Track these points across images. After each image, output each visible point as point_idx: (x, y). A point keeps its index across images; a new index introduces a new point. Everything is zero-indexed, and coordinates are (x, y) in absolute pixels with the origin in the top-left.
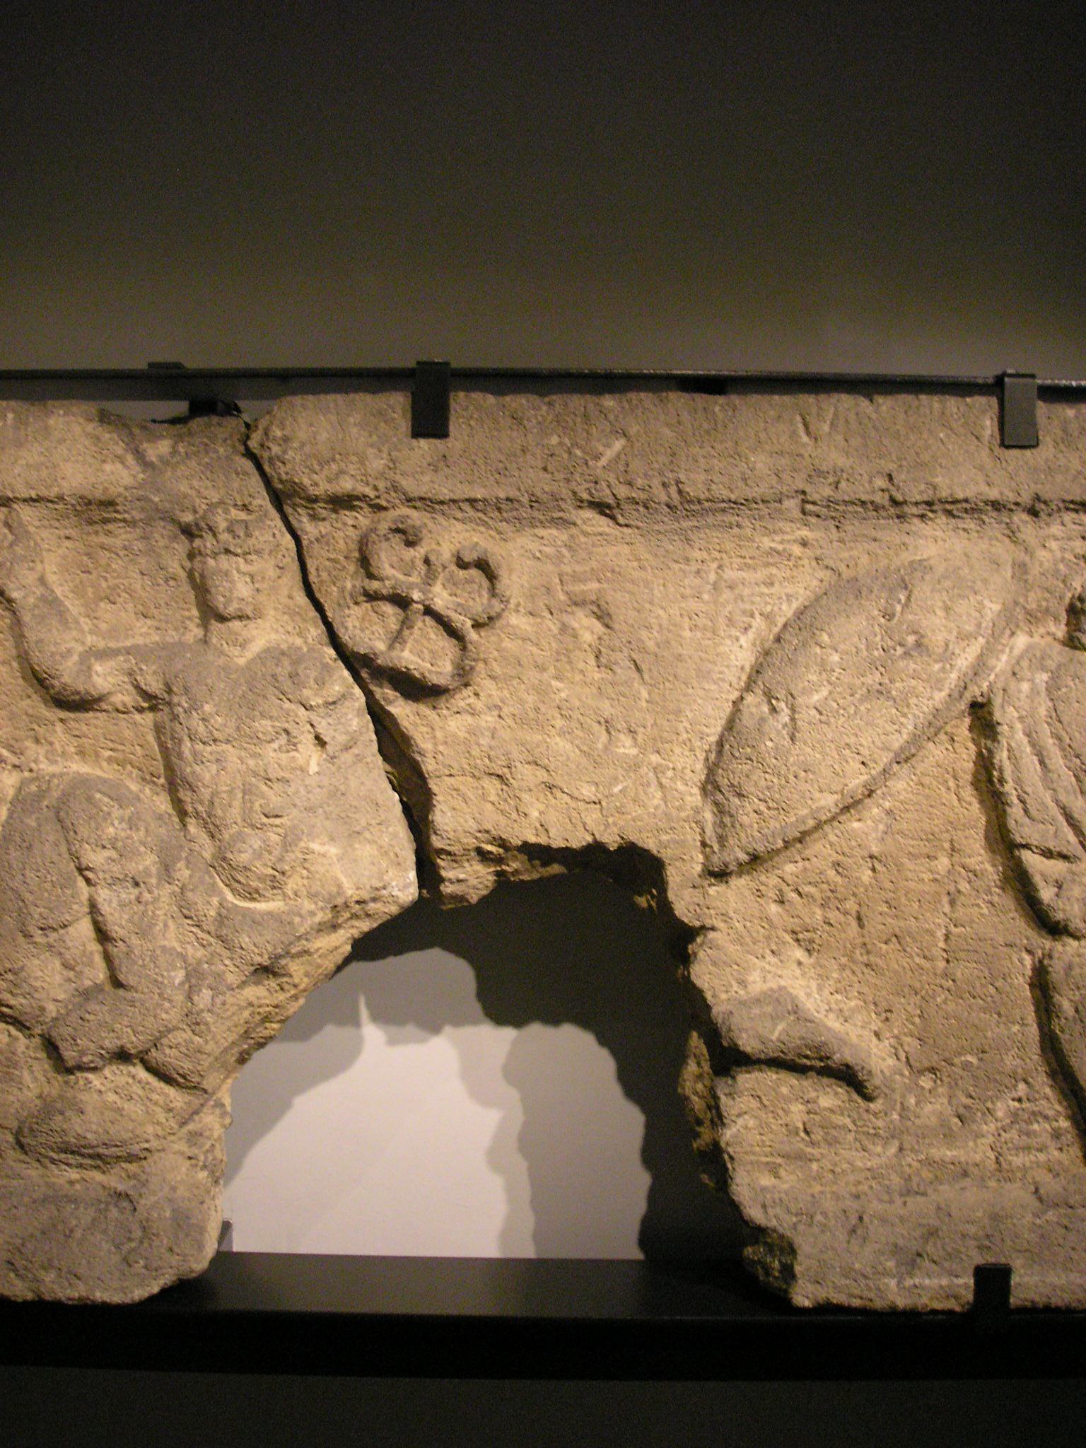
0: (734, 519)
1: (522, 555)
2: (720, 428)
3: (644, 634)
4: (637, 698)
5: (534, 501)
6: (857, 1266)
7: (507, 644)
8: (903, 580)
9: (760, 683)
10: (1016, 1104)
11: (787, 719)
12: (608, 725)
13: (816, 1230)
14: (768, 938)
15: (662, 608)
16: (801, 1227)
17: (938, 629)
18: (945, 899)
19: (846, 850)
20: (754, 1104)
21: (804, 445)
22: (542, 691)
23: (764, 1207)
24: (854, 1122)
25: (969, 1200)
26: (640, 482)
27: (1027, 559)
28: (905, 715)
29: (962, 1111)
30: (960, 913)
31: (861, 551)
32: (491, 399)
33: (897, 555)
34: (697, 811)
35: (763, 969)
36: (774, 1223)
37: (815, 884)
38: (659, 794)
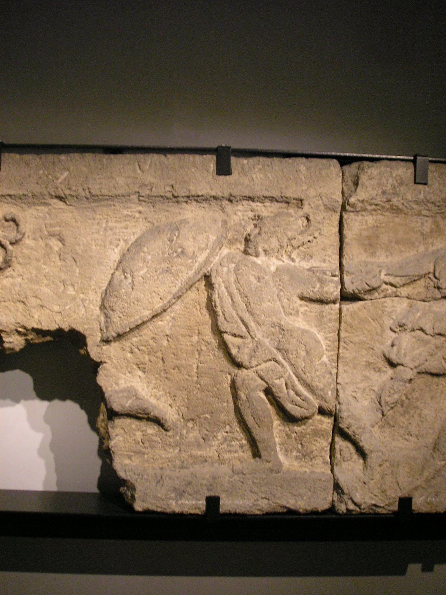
0: (112, 203)
1: (30, 217)
2: (105, 167)
3: (77, 248)
4: (75, 272)
5: (34, 196)
6: (159, 495)
7: (25, 251)
8: (177, 227)
9: (121, 266)
10: (226, 434)
11: (130, 281)
12: (64, 282)
13: (144, 481)
14: (127, 367)
15: (84, 237)
16: (138, 480)
17: (190, 246)
18: (196, 353)
19: (157, 333)
20: (122, 431)
21: (139, 174)
22: (39, 269)
23: (125, 471)
24: (161, 440)
25: (204, 471)
26: (74, 188)
27: (227, 219)
29: (204, 436)
30: (202, 358)
31: (163, 216)
32: (18, 156)
33: (176, 217)
34: (98, 316)
35: (125, 379)
36: (129, 478)
37: (145, 346)
38: (83, 310)
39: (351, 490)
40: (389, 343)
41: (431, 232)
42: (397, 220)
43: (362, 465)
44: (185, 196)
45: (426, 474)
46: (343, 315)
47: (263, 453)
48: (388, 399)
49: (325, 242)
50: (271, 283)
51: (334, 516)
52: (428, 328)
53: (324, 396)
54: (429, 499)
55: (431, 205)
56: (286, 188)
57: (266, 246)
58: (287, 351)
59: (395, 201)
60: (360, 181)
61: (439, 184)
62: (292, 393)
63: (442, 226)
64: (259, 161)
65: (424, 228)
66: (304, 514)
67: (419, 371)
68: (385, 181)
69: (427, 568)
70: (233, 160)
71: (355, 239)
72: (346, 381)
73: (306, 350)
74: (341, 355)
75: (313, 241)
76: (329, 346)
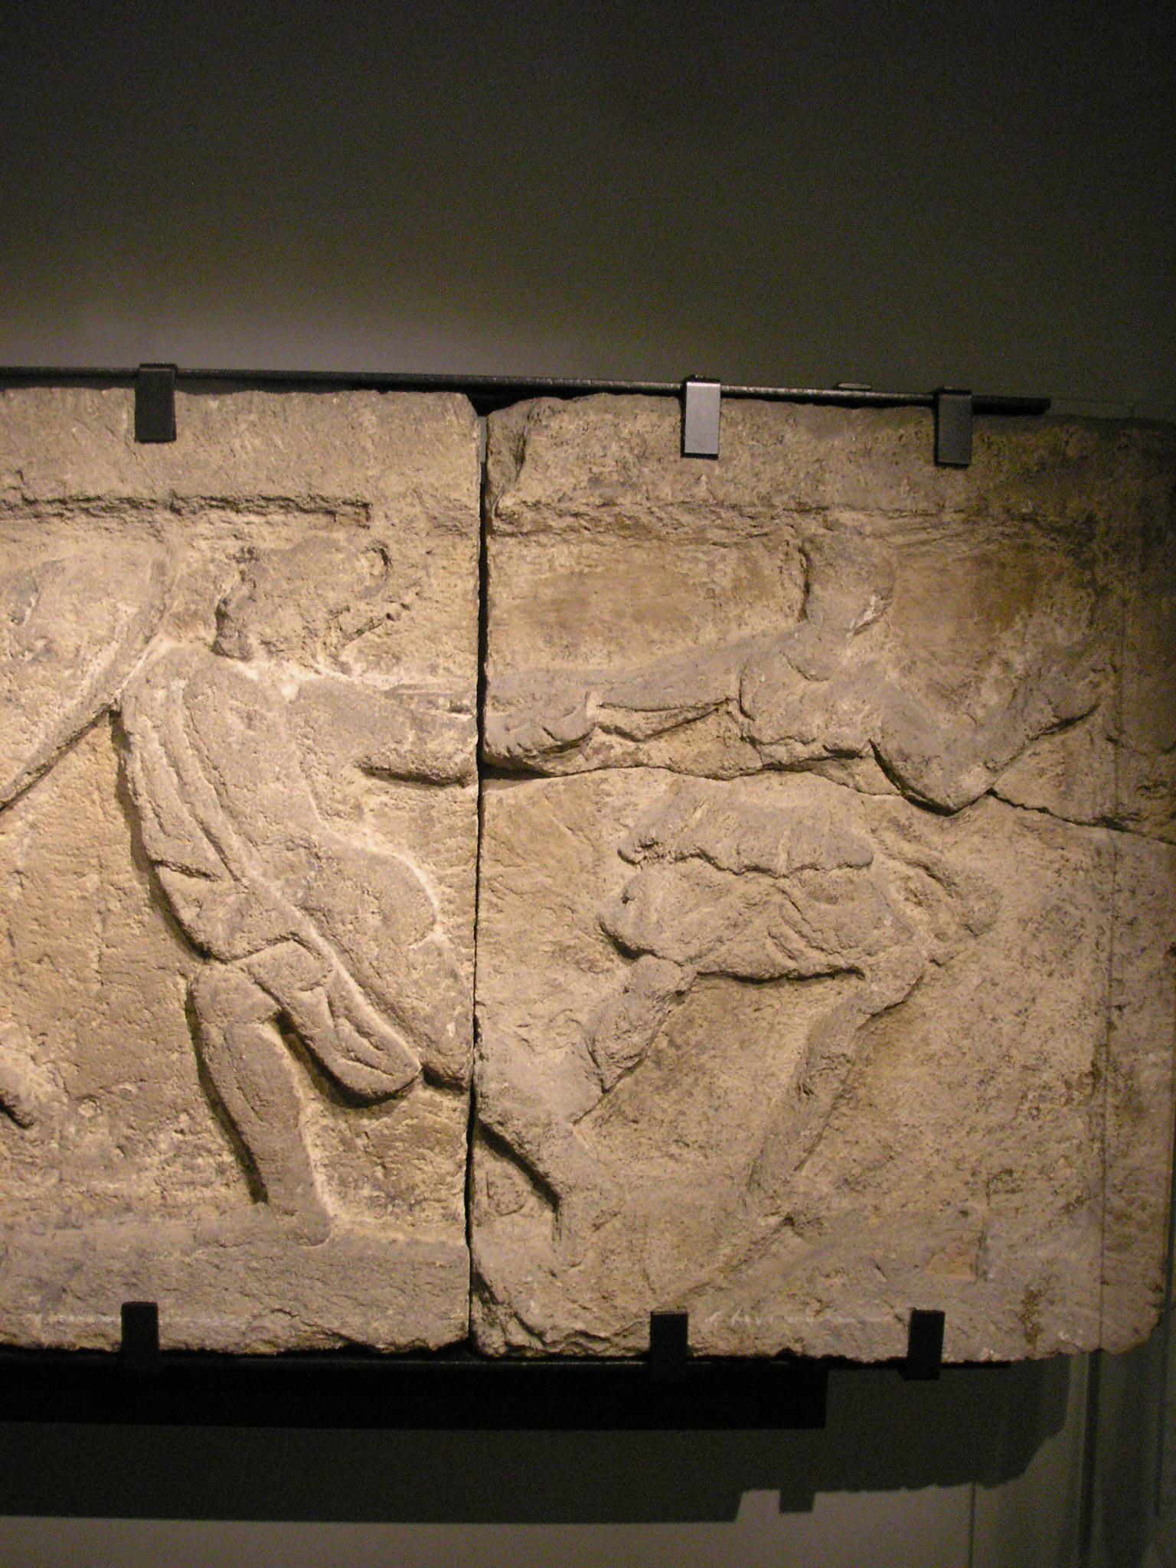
10: (180, 1136)
17: (67, 632)
18: (96, 918)
24: (9, 1149)
25: (117, 1236)
28: (35, 724)
29: (123, 1141)
39: (513, 1293)
40: (617, 892)
41: (735, 588)
42: (638, 556)
43: (550, 1226)
44: (54, 501)
45: (726, 1250)
46: (487, 815)
47: (272, 1189)
48: (614, 1047)
49: (436, 618)
50: (281, 729)
51: (476, 1363)
52: (722, 850)
53: (433, 1038)
54: (735, 1317)
55: (731, 514)
56: (324, 473)
57: (268, 630)
58: (328, 913)
59: (627, 503)
60: (529, 451)
61: (752, 455)
62: (347, 1027)
63: (766, 572)
64: (250, 402)
65: (717, 576)
66: (392, 1356)
67: (703, 970)
68: (598, 450)
69: (796, 1501)
70: (180, 398)
71: (517, 607)
72: (500, 997)
73: (381, 911)
74: (483, 925)
75: (399, 615)
76: (450, 902)
